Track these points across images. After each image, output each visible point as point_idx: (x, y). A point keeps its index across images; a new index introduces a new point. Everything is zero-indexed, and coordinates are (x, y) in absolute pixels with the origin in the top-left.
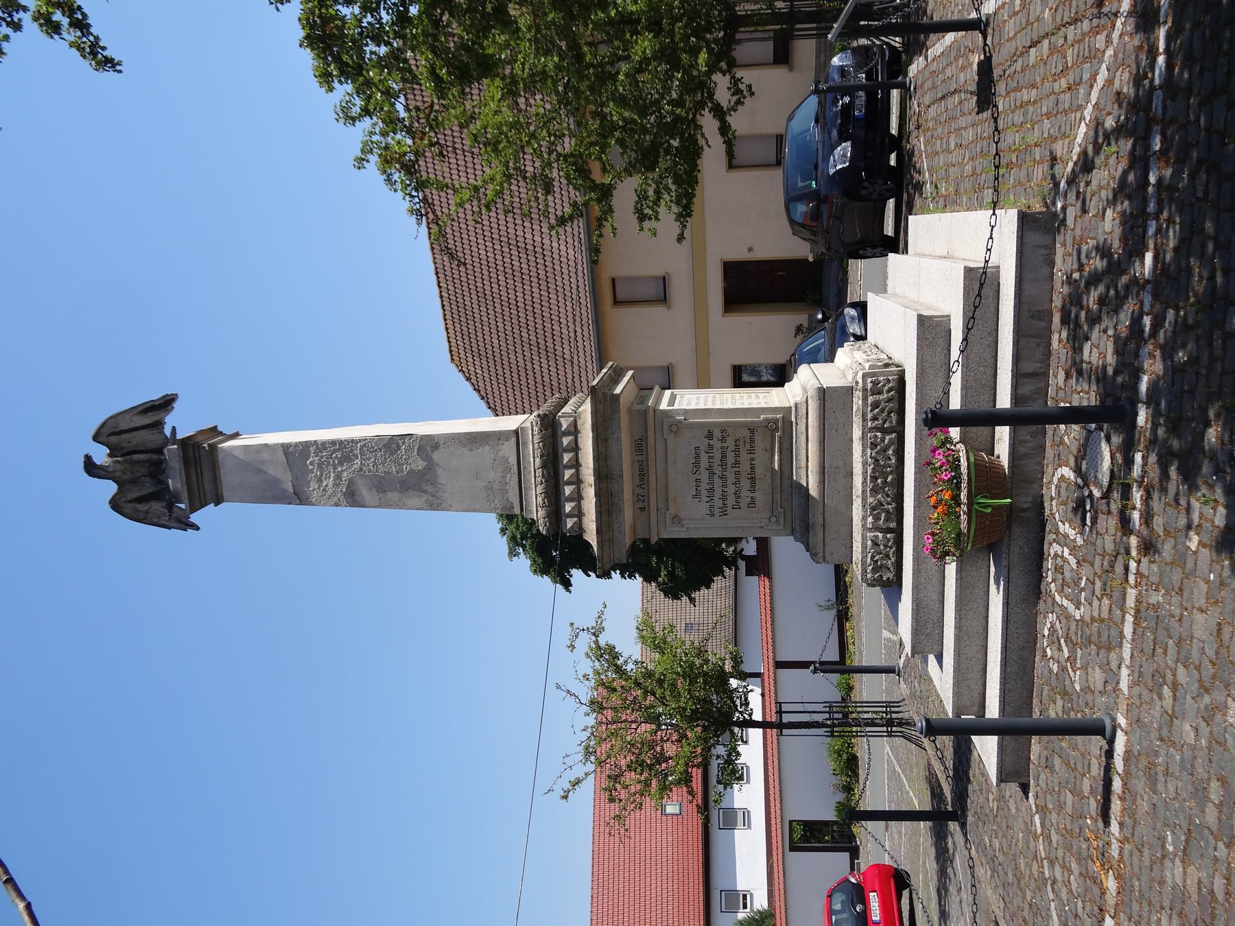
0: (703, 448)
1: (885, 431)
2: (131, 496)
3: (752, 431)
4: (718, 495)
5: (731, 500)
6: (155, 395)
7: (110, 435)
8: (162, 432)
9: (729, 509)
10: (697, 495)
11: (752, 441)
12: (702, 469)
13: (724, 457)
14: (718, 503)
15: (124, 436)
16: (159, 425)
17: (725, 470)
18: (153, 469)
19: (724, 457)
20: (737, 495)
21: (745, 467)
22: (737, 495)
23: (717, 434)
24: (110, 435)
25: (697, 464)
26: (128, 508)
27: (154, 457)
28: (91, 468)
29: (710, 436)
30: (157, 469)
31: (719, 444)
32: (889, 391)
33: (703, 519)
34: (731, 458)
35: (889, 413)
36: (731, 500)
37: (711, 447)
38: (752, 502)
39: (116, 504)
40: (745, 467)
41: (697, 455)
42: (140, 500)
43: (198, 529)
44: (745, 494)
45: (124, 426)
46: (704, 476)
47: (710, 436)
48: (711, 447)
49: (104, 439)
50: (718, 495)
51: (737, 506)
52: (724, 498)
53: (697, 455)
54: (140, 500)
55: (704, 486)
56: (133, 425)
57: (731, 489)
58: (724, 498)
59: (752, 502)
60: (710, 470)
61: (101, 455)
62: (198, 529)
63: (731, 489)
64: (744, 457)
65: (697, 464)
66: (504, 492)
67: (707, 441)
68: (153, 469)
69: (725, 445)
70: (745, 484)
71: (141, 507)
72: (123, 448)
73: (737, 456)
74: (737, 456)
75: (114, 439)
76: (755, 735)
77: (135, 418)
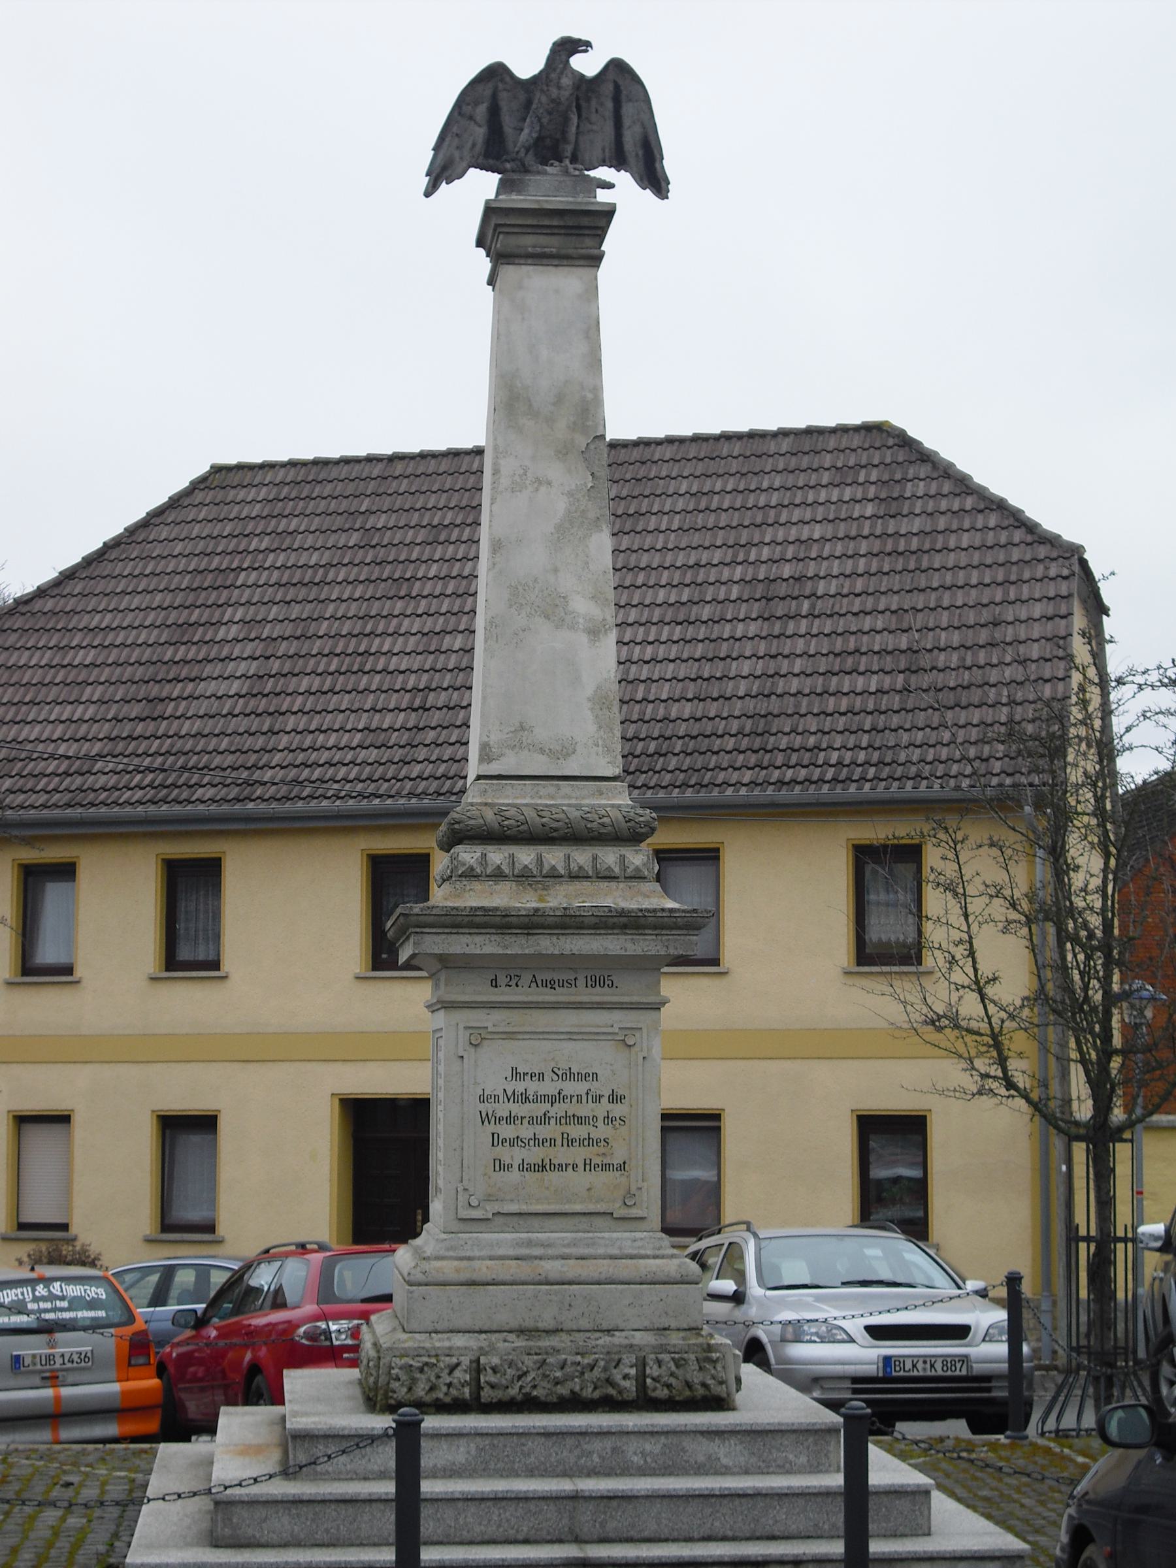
0: (595, 1087)
1: (641, 1377)
2: (503, 96)
3: (622, 1167)
4: (517, 1109)
5: (507, 1131)
6: (670, 165)
7: (617, 87)
8: (603, 163)
9: (491, 1128)
10: (516, 1074)
11: (606, 1167)
12: (560, 1085)
13: (581, 1120)
14: (503, 1109)
15: (610, 105)
16: (619, 162)
17: (559, 1121)
18: (548, 142)
19: (581, 1120)
20: (515, 1142)
21: (562, 1155)
22: (515, 1142)
23: (618, 1110)
24: (617, 87)
25: (569, 1075)
26: (486, 90)
27: (569, 149)
28: (568, 47)
29: (615, 1098)
30: (549, 149)
31: (601, 1115)
32: (704, 1385)
33: (476, 1083)
34: (578, 1131)
35: (669, 1386)
36: (507, 1131)
37: (598, 1099)
38: (501, 1166)
39: (495, 74)
40: (562, 1155)
41: (584, 1077)
42: (494, 112)
43: (428, 194)
44: (516, 1155)
45: (628, 110)
46: (549, 1087)
47: (615, 1098)
48: (598, 1099)
49: (611, 76)
50: (517, 1109)
51: (496, 1140)
52: (510, 1119)
53: (584, 1077)
54: (494, 112)
55: (533, 1087)
56: (627, 122)
57: (526, 1132)
58: (510, 1119)
59: (501, 1166)
60: (559, 1098)
61: (587, 65)
62: (428, 194)
63: (526, 1132)
64: (578, 1154)
65: (569, 1075)
66: (517, 746)
67: (607, 1093)
68: (548, 142)
69: (600, 1123)
70: (535, 1155)
71: (481, 111)
72: (588, 100)
73: (581, 1142)
74: (581, 1142)
75: (608, 89)
76: (1120, 1246)
77: (638, 129)
